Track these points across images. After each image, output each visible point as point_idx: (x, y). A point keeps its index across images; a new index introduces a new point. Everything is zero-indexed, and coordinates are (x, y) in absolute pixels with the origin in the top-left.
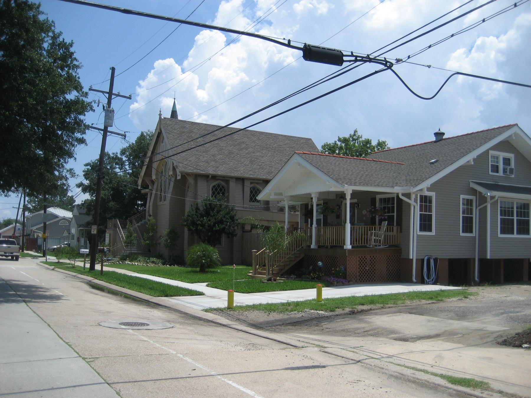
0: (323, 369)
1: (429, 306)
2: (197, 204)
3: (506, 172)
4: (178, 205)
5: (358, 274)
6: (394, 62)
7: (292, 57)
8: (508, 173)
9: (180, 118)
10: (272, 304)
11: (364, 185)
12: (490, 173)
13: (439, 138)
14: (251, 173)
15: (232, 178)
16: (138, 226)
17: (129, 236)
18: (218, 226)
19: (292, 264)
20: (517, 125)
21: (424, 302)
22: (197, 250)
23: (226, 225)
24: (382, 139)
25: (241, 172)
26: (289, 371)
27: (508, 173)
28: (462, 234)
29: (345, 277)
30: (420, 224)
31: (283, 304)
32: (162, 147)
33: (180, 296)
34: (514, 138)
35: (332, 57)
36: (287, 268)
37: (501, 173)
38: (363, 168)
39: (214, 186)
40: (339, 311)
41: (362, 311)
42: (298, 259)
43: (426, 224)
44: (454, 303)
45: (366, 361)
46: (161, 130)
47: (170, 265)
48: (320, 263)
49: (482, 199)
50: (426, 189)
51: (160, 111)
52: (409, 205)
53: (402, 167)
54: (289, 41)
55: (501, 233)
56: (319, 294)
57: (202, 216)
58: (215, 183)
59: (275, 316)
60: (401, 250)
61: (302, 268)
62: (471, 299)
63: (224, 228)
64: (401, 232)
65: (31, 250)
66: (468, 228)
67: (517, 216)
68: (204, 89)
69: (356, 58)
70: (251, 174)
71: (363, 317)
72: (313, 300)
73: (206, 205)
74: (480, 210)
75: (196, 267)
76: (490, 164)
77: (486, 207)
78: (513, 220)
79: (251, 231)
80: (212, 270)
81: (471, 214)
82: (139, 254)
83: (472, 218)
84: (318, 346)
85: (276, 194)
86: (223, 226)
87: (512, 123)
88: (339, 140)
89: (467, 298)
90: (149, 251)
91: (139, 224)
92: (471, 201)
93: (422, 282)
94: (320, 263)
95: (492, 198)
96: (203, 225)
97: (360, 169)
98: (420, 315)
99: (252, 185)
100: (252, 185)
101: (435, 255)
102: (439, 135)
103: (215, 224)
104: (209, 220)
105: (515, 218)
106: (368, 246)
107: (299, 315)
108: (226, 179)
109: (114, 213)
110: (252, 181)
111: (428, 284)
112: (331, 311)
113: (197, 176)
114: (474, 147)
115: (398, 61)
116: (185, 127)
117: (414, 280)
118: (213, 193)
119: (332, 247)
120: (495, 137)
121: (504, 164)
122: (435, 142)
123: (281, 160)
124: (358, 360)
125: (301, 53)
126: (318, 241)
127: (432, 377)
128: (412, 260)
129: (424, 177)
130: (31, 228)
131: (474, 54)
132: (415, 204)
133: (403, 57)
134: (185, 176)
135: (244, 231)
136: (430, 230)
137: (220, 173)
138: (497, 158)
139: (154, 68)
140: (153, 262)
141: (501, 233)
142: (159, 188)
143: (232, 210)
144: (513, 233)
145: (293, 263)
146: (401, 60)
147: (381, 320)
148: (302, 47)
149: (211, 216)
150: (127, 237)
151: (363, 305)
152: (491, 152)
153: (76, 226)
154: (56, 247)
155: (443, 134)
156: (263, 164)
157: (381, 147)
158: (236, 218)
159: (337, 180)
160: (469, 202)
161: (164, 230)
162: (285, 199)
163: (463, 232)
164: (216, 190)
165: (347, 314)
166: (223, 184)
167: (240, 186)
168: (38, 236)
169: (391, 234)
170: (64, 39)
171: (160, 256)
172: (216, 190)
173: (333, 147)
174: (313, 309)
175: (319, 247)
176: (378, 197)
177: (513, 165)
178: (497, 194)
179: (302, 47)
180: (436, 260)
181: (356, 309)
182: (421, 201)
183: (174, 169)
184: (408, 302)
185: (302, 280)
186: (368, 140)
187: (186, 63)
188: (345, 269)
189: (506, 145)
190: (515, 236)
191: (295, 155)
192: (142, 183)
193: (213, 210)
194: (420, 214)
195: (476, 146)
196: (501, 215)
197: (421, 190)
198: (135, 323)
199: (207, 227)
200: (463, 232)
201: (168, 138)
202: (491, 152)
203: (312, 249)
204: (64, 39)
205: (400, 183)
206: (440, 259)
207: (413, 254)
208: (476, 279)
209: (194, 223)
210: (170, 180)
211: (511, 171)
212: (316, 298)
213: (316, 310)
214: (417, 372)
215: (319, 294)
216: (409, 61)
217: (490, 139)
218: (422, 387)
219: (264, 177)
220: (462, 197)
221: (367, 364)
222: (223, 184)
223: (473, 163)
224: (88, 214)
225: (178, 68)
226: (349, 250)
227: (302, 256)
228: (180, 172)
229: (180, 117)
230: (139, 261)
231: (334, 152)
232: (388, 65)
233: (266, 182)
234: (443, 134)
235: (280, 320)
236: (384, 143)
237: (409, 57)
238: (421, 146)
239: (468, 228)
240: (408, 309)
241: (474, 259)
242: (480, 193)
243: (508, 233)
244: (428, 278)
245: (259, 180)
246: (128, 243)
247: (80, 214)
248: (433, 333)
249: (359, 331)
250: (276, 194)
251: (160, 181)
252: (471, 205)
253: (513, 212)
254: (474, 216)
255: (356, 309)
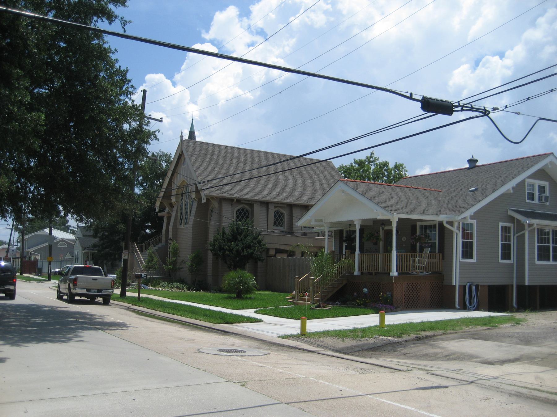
0: (446, 389)
1: (487, 332)
2: (223, 229)
3: (541, 200)
4: (201, 229)
5: (404, 300)
6: (490, 110)
7: (416, 108)
8: (543, 201)
9: (198, 139)
10: (340, 331)
11: (411, 213)
12: (527, 201)
13: (473, 165)
14: (275, 196)
15: (256, 201)
16: (156, 250)
17: (151, 260)
18: (246, 250)
19: (336, 290)
20: (552, 154)
21: (479, 328)
22: (232, 277)
23: (254, 250)
24: (399, 162)
25: (265, 196)
26: (421, 391)
27: (543, 201)
28: (501, 261)
29: (392, 304)
30: (463, 251)
31: (350, 331)
32: (182, 169)
33: (240, 323)
34: (550, 166)
35: (444, 108)
36: (330, 295)
37: (536, 201)
38: (405, 196)
39: (238, 210)
40: (405, 337)
41: (427, 337)
42: (341, 286)
43: (467, 252)
44: (507, 328)
45: (479, 382)
46: (182, 152)
47: (196, 290)
48: (365, 290)
49: (520, 227)
50: (469, 217)
51: (182, 133)
52: (452, 232)
53: (441, 193)
54: (411, 94)
55: (538, 260)
56: (382, 320)
57: (229, 241)
58: (240, 207)
59: (349, 343)
60: (443, 276)
61: (345, 296)
62: (524, 325)
63: (252, 253)
64: (443, 258)
65: (30, 273)
66: (506, 255)
67: (553, 243)
68: (195, 103)
69: (462, 108)
70: (275, 198)
71: (431, 343)
72: (376, 326)
73: (233, 230)
74: (517, 237)
75: (233, 293)
76: (527, 191)
77: (524, 234)
78: (549, 247)
79: (275, 256)
80: (249, 296)
81: (509, 241)
82: (161, 278)
83: (510, 245)
84: (425, 370)
85: (316, 221)
86: (252, 251)
87: (548, 152)
88: (355, 162)
89: (519, 324)
90: (170, 275)
91: (156, 248)
92: (509, 228)
93: (464, 308)
94: (365, 290)
95: (530, 225)
96: (231, 250)
97: (403, 196)
98: (485, 340)
99: (276, 209)
100: (276, 209)
101: (477, 282)
102: (472, 162)
103: (243, 249)
104: (237, 245)
105: (551, 245)
106: (410, 272)
107: (372, 341)
108: (251, 203)
109: (121, 235)
110: (276, 205)
111: (470, 310)
112: (399, 337)
113: (222, 200)
114: (513, 176)
115: (494, 109)
116: (206, 149)
117: (457, 306)
118: (238, 217)
119: (376, 274)
120: (532, 166)
121: (539, 191)
122: (468, 169)
123: (303, 184)
124: (470, 380)
125: (419, 104)
126: (361, 268)
127: (548, 395)
128: (455, 286)
129: (466, 205)
130: (27, 250)
131: (480, 70)
132: (458, 231)
133: (501, 105)
134: (209, 199)
135: (268, 256)
136: (471, 257)
137: (244, 197)
138: (533, 186)
139: (145, 82)
140: (177, 287)
141: (538, 260)
142: (179, 210)
143: (260, 234)
144: (549, 260)
145: (336, 290)
146: (497, 109)
147: (454, 345)
148: (420, 99)
149: (239, 241)
150: (149, 262)
151: (424, 331)
152: (528, 180)
153: (81, 248)
154: (57, 270)
155: (477, 161)
156: (287, 188)
157: (398, 170)
158: (263, 242)
159: (385, 208)
160: (506, 230)
161: (186, 254)
162: (325, 225)
163: (502, 259)
164: (240, 213)
165: (413, 340)
166: (247, 207)
167: (264, 210)
168: (35, 258)
169: (434, 260)
170: (120, 67)
171: (182, 282)
172: (240, 213)
173: (349, 169)
174: (381, 335)
175: (362, 273)
176: (418, 224)
177: (547, 193)
178: (536, 222)
179: (420, 99)
180: (477, 287)
181: (422, 335)
182: (463, 229)
183: (198, 191)
184: (465, 328)
185: (349, 307)
186: (386, 162)
187: (177, 77)
188: (392, 296)
189: (541, 174)
190: (551, 262)
191: (339, 182)
192: (160, 205)
193: (240, 234)
194: (463, 241)
195: (515, 175)
196: (538, 242)
197: (465, 218)
198: (231, 350)
199: (234, 252)
200: (502, 259)
201: (191, 161)
202: (528, 180)
203: (355, 276)
204: (120, 67)
205: (444, 211)
206: (481, 286)
207: (456, 281)
208: (515, 305)
209: (221, 248)
210: (192, 204)
211: (547, 199)
212: (378, 324)
213: (385, 336)
214: (533, 391)
215: (382, 320)
216: (506, 110)
217: (528, 168)
218: (545, 403)
219: (289, 201)
220: (501, 224)
221: (481, 384)
222: (247, 207)
223: (512, 191)
224: (95, 236)
225: (168, 82)
226: (395, 277)
227: (345, 282)
228: (206, 196)
229: (199, 137)
230: (163, 286)
231: (350, 174)
232: (486, 113)
233: (306, 208)
234: (477, 161)
235: (358, 346)
236: (402, 165)
237: (506, 107)
238: (454, 172)
239: (506, 255)
240: (470, 334)
241: (512, 286)
242: (518, 221)
243: (544, 260)
244: (470, 305)
245: (283, 204)
246: (150, 268)
247: (84, 236)
248: (511, 357)
249: (439, 356)
250: (316, 221)
251: (180, 204)
252: (509, 233)
253: (549, 239)
254: (512, 243)
255: (422, 335)
